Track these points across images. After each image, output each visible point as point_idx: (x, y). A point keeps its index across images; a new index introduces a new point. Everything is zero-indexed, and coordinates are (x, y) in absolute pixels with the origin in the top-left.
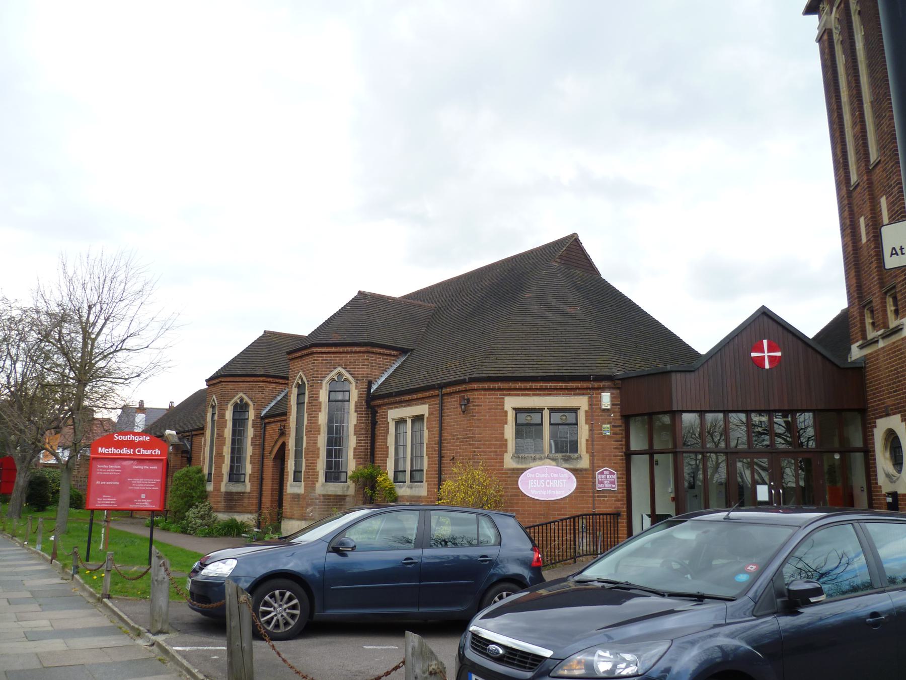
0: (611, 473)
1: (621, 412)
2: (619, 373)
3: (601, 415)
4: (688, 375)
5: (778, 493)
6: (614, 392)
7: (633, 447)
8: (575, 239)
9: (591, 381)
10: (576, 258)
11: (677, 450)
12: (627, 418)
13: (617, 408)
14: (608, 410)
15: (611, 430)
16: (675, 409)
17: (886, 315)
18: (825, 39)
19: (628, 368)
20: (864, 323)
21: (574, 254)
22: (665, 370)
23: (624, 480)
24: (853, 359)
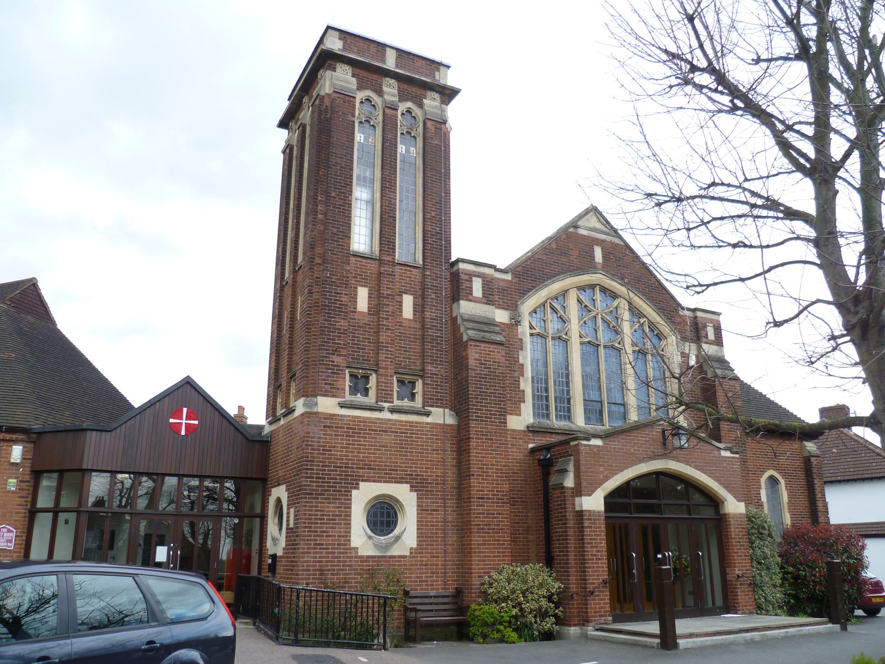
0: (9, 531)
1: (31, 467)
2: (36, 426)
3: (8, 469)
4: (104, 434)
5: (175, 553)
6: (28, 445)
7: (40, 505)
8: (34, 284)
9: (3, 432)
10: (30, 303)
11: (81, 509)
12: (37, 475)
13: (28, 463)
14: (17, 464)
15: (17, 485)
16: (84, 467)
17: (289, 397)
18: (288, 150)
19: (50, 423)
20: (276, 402)
21: (29, 299)
22: (81, 428)
23: (24, 538)
24: (265, 433)
